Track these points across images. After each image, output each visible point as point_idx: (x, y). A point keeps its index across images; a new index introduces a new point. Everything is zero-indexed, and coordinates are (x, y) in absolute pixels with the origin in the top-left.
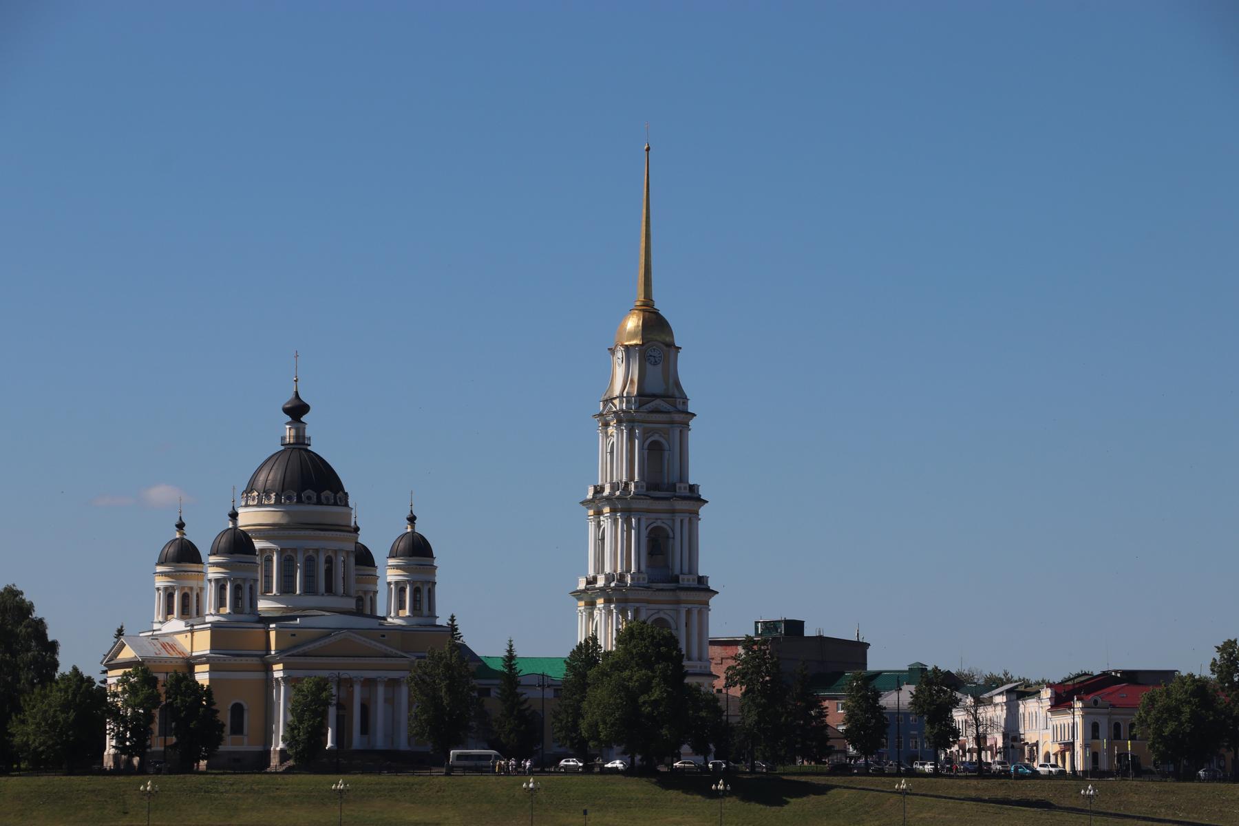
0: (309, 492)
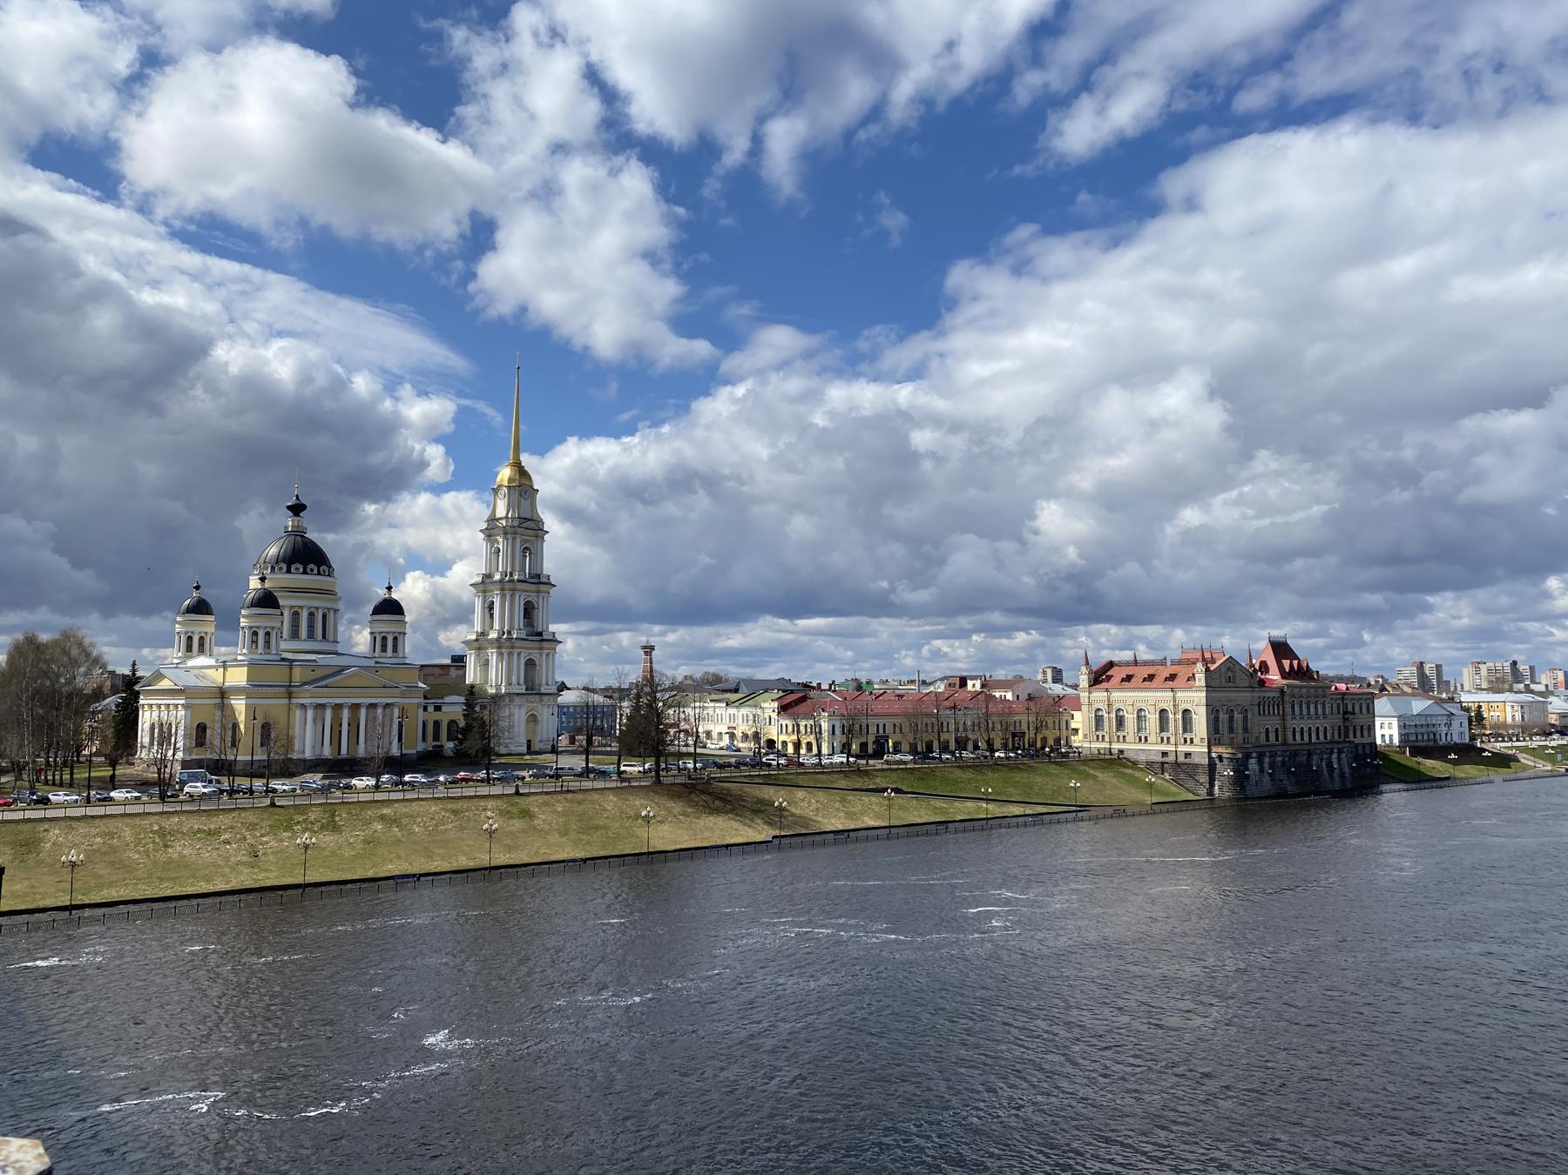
0: (312, 566)
